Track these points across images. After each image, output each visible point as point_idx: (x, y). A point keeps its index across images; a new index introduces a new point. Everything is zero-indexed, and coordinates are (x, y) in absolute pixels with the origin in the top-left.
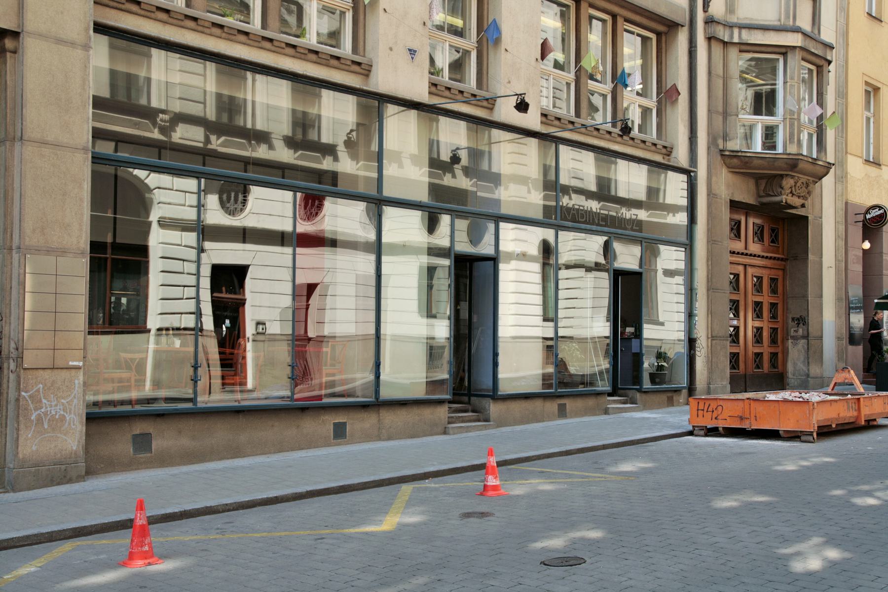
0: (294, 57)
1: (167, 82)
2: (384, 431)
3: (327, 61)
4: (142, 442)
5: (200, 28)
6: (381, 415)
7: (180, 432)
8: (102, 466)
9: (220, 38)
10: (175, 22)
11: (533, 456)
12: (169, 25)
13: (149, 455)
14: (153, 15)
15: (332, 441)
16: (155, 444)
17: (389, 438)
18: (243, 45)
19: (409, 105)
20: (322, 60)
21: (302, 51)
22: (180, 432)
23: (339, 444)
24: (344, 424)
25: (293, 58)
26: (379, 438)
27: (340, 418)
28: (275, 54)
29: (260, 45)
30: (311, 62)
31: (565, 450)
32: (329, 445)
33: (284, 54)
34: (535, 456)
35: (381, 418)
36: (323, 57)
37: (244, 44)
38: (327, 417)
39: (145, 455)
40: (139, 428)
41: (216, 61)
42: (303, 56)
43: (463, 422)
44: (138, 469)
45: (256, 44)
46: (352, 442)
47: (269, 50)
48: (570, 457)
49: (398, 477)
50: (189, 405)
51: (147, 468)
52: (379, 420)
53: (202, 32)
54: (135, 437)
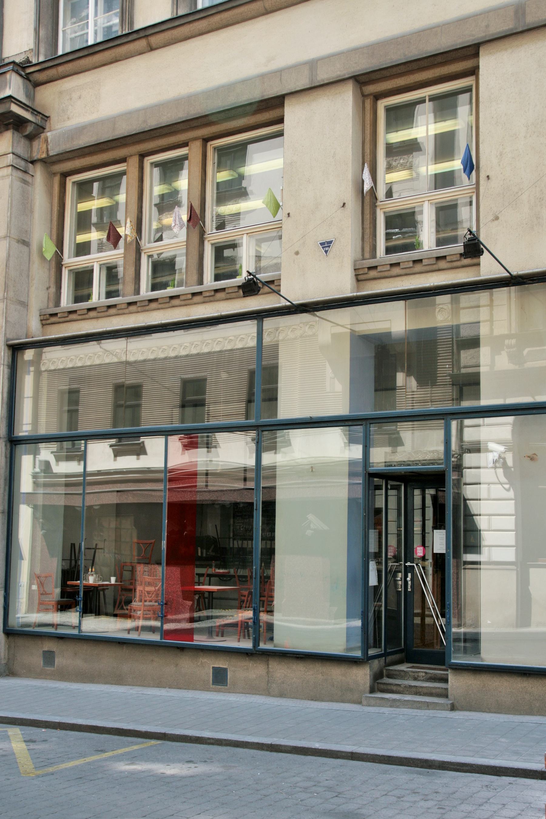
0: (204, 302)
1: (479, 322)
2: (274, 685)
3: (237, 293)
4: (49, 657)
5: (121, 312)
6: (270, 666)
7: (76, 654)
8: (25, 671)
9: (139, 312)
10: (102, 314)
11: (209, 739)
12: (101, 319)
13: (53, 669)
14: (87, 316)
15: (211, 686)
16: (58, 661)
17: (282, 695)
18: (185, 307)
19: (296, 310)
20: (232, 294)
21: (208, 294)
22: (76, 654)
23: (219, 691)
24: (225, 670)
25: (204, 304)
26: (268, 693)
27: (221, 663)
28: (188, 307)
29: (170, 305)
30: (223, 300)
31: (269, 742)
32: (208, 690)
33: (195, 304)
34: (213, 739)
35: (271, 670)
36: (230, 291)
37: (159, 309)
38: (205, 660)
39: (50, 668)
40: (48, 645)
41: (96, 339)
42: (211, 298)
43: (417, 693)
44: (46, 679)
45: (167, 305)
46: (233, 691)
47: (180, 306)
48: (275, 754)
49: (30, 720)
50: (75, 632)
51: (51, 679)
52: (268, 673)
53: (124, 314)
54: (45, 652)
